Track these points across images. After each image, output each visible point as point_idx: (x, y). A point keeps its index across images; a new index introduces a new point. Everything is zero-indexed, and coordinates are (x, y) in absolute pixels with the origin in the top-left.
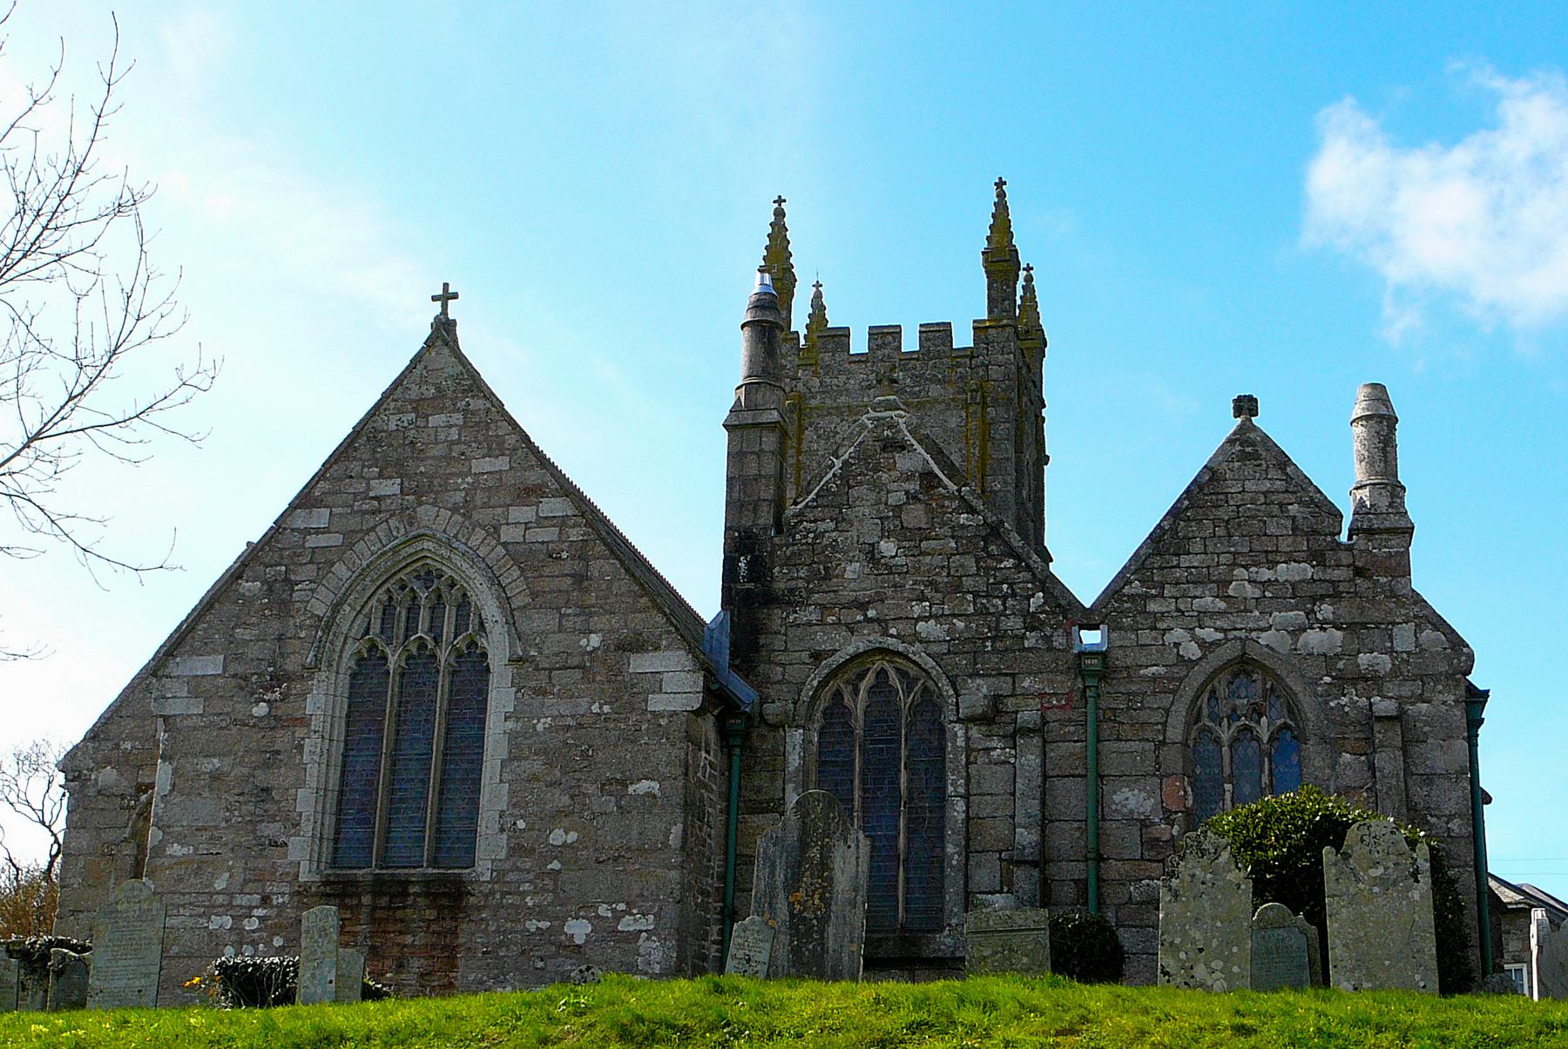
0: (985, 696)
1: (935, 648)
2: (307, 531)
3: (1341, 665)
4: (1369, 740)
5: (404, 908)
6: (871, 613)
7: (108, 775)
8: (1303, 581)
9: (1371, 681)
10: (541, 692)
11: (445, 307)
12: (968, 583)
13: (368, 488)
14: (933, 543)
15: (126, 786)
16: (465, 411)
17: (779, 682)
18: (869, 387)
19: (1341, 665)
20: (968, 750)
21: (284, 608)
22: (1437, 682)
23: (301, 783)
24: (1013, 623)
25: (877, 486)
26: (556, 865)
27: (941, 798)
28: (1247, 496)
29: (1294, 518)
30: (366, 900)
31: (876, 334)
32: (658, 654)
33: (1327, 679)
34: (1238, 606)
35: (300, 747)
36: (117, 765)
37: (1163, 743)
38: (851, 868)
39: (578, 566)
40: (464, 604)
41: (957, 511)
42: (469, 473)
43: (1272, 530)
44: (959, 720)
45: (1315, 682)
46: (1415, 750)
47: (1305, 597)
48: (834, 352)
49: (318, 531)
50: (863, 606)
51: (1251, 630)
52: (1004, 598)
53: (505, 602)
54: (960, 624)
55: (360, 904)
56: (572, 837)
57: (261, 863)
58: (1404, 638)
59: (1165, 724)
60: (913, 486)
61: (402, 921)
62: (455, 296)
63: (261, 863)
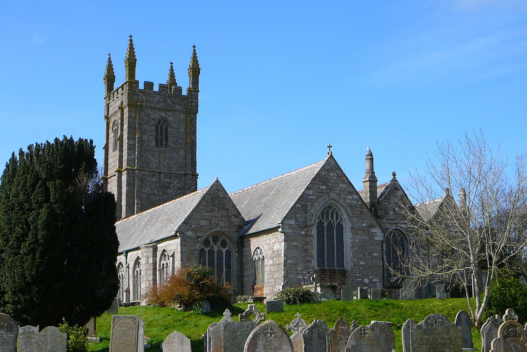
2: (308, 195)
7: (189, 233)
15: (194, 236)
18: (160, 102)
26: (361, 268)
30: (328, 273)
35: (312, 241)
36: (192, 231)
39: (361, 210)
48: (150, 89)
49: (310, 195)
50: (393, 220)
56: (364, 263)
57: (307, 265)
63: (307, 265)
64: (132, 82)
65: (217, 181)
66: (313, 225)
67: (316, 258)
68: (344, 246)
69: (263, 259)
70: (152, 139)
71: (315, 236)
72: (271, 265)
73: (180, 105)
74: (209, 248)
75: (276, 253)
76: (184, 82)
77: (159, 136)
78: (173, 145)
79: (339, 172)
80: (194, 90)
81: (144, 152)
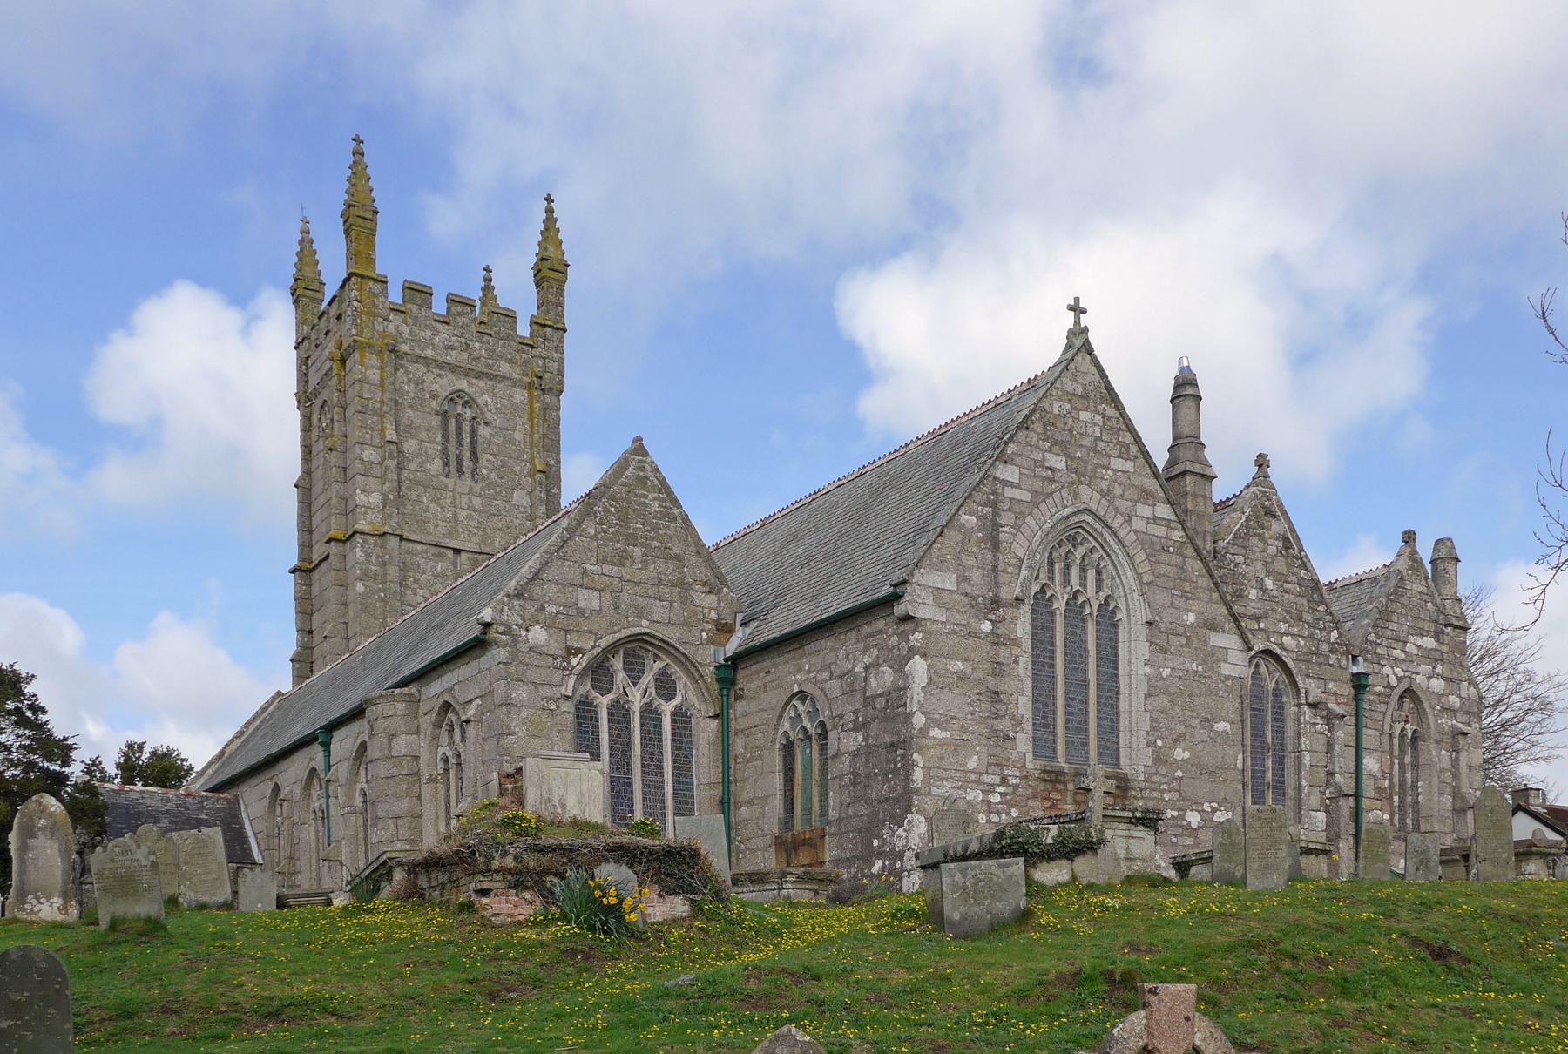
15: (556, 648)
18: (451, 348)
26: (1179, 773)
35: (1016, 662)
36: (547, 627)
39: (1179, 560)
49: (1013, 485)
50: (1258, 619)
56: (1187, 755)
57: (998, 751)
63: (998, 751)
64: (361, 274)
65: (639, 449)
66: (1019, 600)
67: (1028, 727)
68: (1123, 689)
69: (823, 737)
71: (1027, 644)
72: (855, 755)
73: (510, 362)
74: (611, 696)
75: (881, 703)
76: (518, 293)
77: (452, 447)
78: (494, 476)
79: (1111, 412)
80: (550, 324)
81: (409, 489)
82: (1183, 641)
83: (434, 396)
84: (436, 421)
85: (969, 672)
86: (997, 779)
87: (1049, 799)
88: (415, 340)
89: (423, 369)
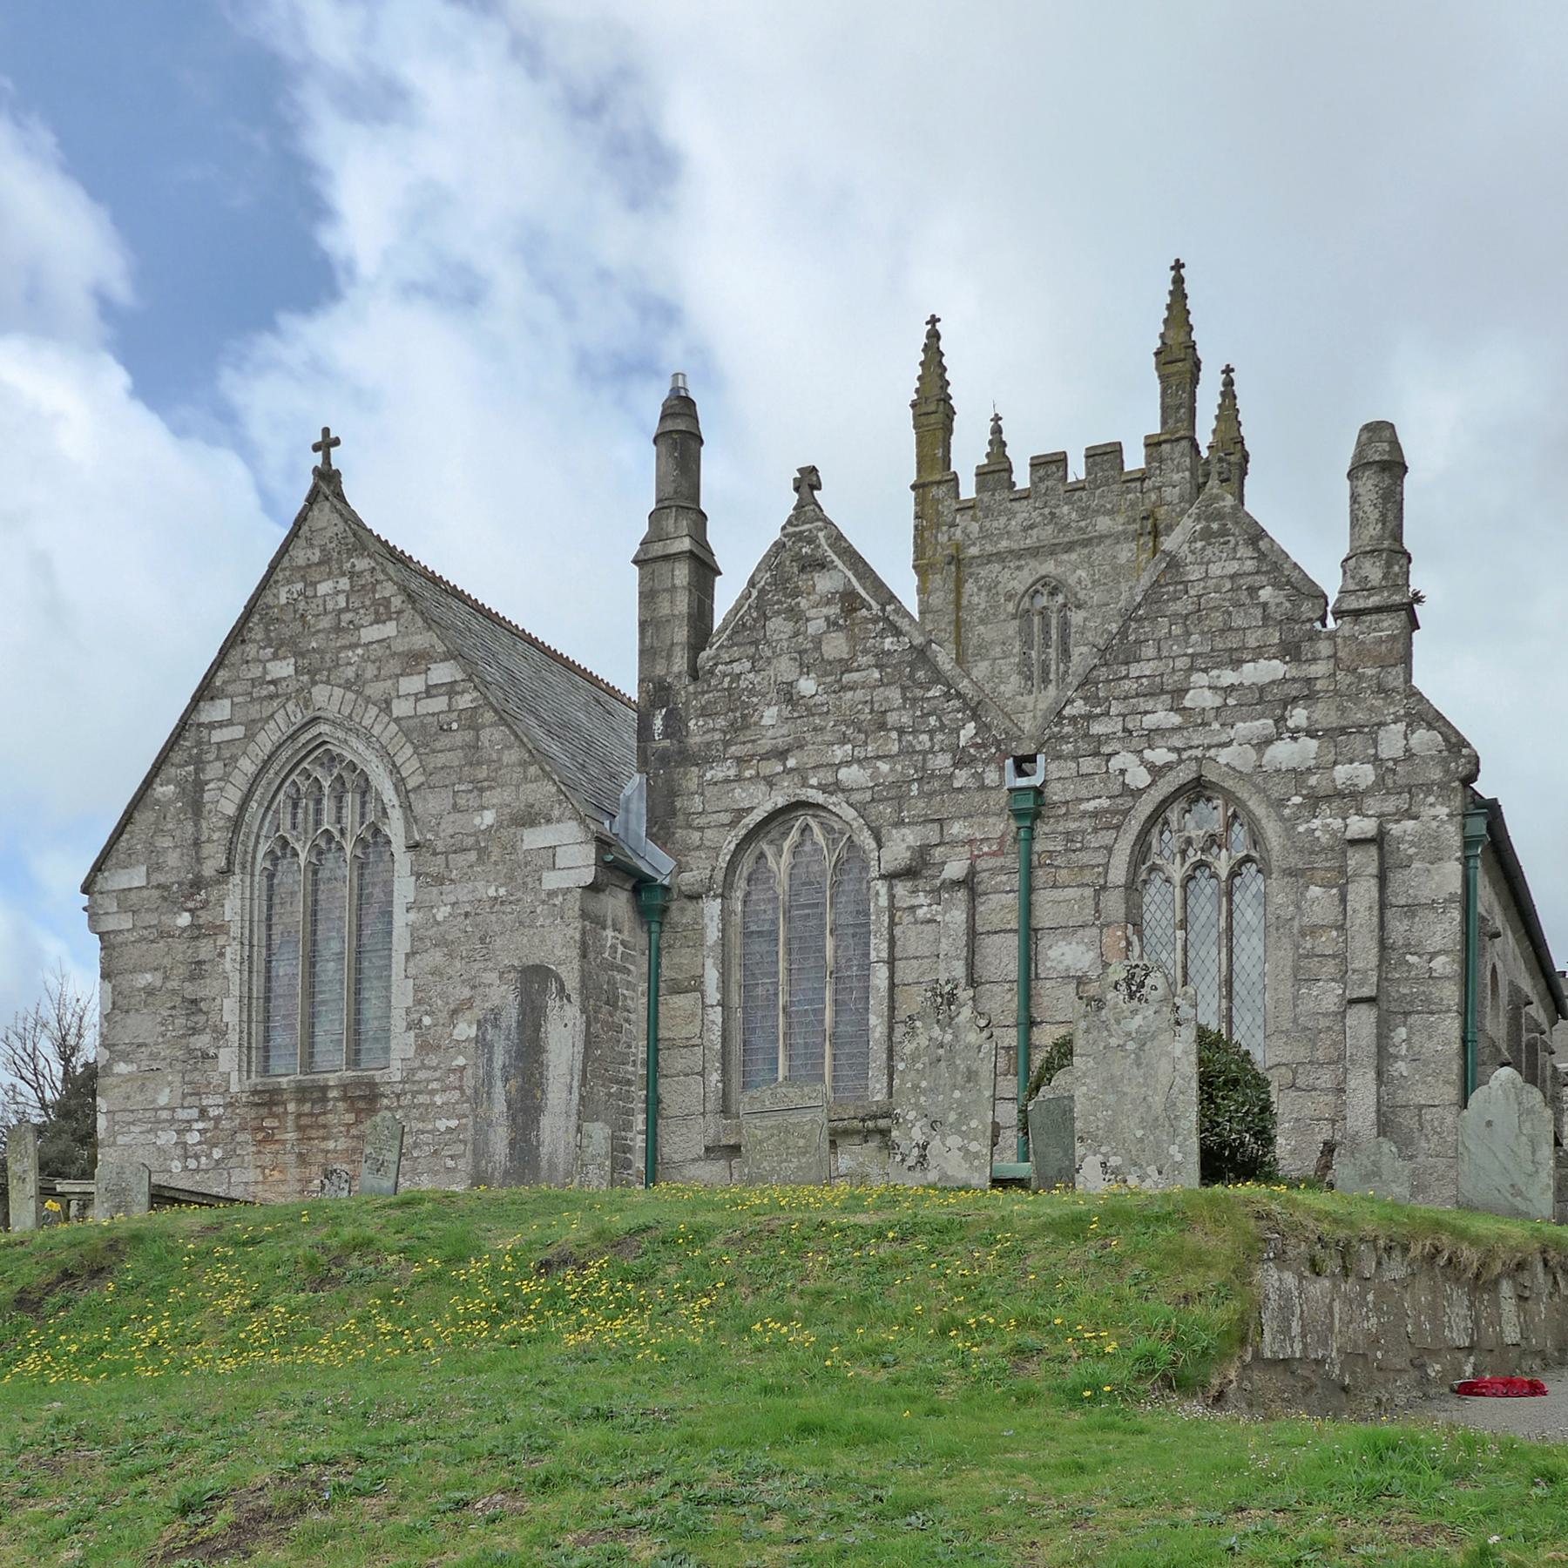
0: (908, 848)
1: (856, 797)
2: (211, 726)
3: (1313, 781)
4: (1342, 870)
5: (325, 1113)
6: (791, 763)
8: (1273, 682)
9: (1351, 798)
10: (440, 880)
11: (327, 458)
12: (892, 718)
13: (265, 672)
14: (855, 676)
16: (353, 575)
17: (698, 848)
18: (1031, 527)
19: (1313, 781)
20: (892, 907)
21: (196, 808)
22: (1429, 793)
23: (227, 994)
24: (942, 761)
25: (795, 614)
27: (866, 967)
28: (1211, 583)
29: (1265, 605)
30: (291, 1107)
31: (1038, 463)
32: (553, 826)
33: (1297, 800)
34: (1196, 720)
35: (222, 955)
37: (1104, 888)
38: (567, 1053)
39: (469, 736)
40: (365, 788)
41: (881, 635)
42: (357, 645)
43: (1238, 622)
44: (882, 877)
45: (1281, 803)
46: (1396, 878)
47: (1272, 702)
50: (782, 755)
51: (1209, 747)
52: (931, 733)
53: (400, 784)
54: (884, 767)
55: (286, 1112)
57: (197, 1076)
58: (1392, 742)
59: (1106, 866)
60: (833, 610)
61: (324, 1126)
62: (337, 442)
63: (197, 1076)
70: (1005, 669)
73: (1111, 513)
82: (473, 856)
83: (1009, 597)
84: (1012, 627)
85: (158, 983)
86: (195, 1113)
87: (262, 1129)
88: (986, 535)
89: (997, 567)
